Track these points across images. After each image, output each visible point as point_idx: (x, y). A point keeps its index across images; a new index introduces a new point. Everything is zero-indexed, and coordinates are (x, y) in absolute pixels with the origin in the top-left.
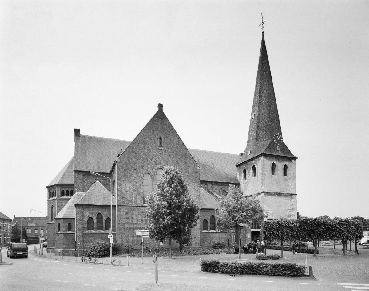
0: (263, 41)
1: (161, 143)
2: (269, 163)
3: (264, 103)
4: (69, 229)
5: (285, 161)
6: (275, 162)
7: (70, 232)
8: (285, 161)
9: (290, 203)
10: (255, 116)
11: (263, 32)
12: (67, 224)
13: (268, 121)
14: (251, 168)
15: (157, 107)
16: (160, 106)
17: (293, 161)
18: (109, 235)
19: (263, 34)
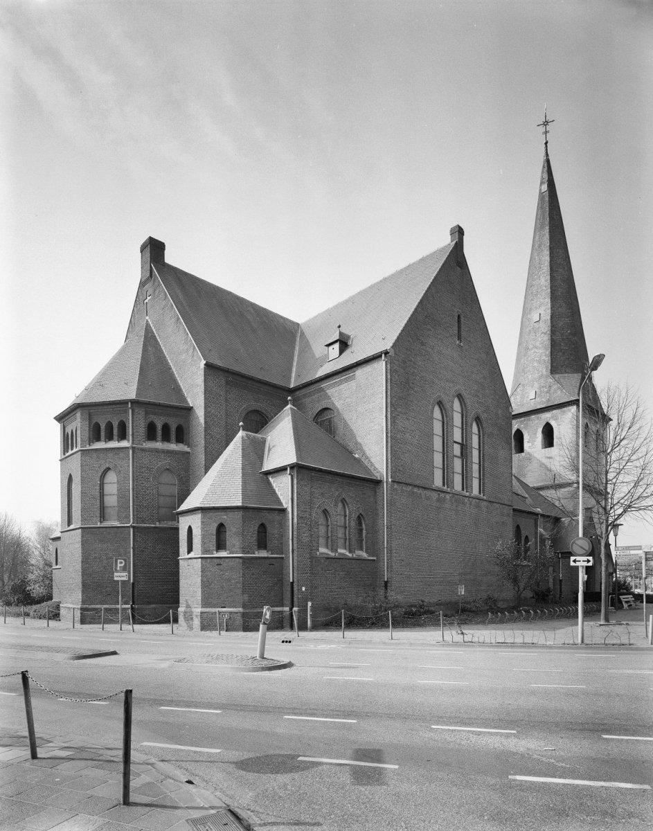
3: (562, 293)
4: (262, 544)
7: (263, 554)
10: (543, 318)
11: (546, 143)
12: (254, 528)
13: (571, 334)
14: (540, 430)
15: (465, 234)
18: (572, 558)
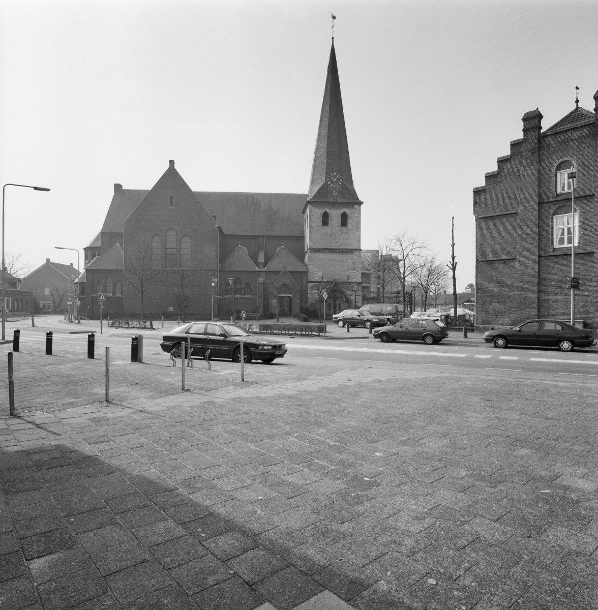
0: (333, 46)
1: (171, 202)
2: (319, 212)
5: (343, 208)
6: (328, 210)
8: (343, 207)
9: (349, 260)
16: (172, 163)
17: (356, 206)
19: (333, 41)
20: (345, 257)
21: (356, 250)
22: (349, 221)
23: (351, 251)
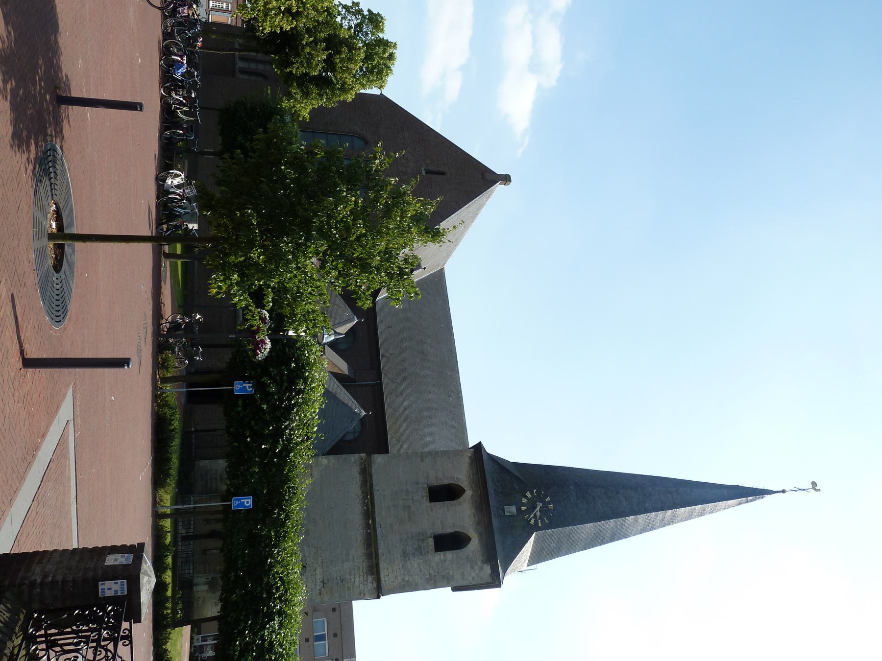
6: (469, 493)
20: (358, 552)
21: (378, 580)
22: (449, 555)
23: (374, 570)
